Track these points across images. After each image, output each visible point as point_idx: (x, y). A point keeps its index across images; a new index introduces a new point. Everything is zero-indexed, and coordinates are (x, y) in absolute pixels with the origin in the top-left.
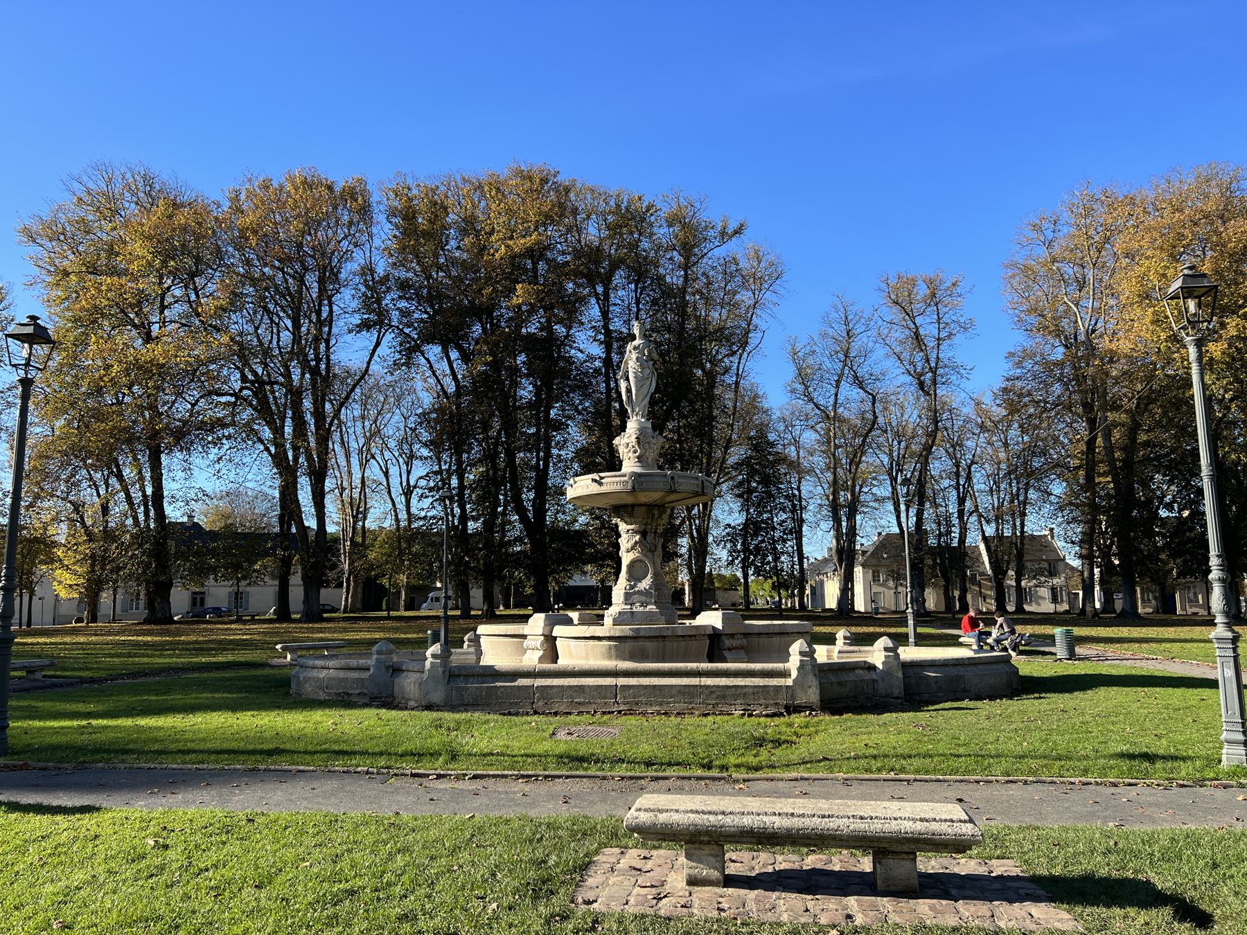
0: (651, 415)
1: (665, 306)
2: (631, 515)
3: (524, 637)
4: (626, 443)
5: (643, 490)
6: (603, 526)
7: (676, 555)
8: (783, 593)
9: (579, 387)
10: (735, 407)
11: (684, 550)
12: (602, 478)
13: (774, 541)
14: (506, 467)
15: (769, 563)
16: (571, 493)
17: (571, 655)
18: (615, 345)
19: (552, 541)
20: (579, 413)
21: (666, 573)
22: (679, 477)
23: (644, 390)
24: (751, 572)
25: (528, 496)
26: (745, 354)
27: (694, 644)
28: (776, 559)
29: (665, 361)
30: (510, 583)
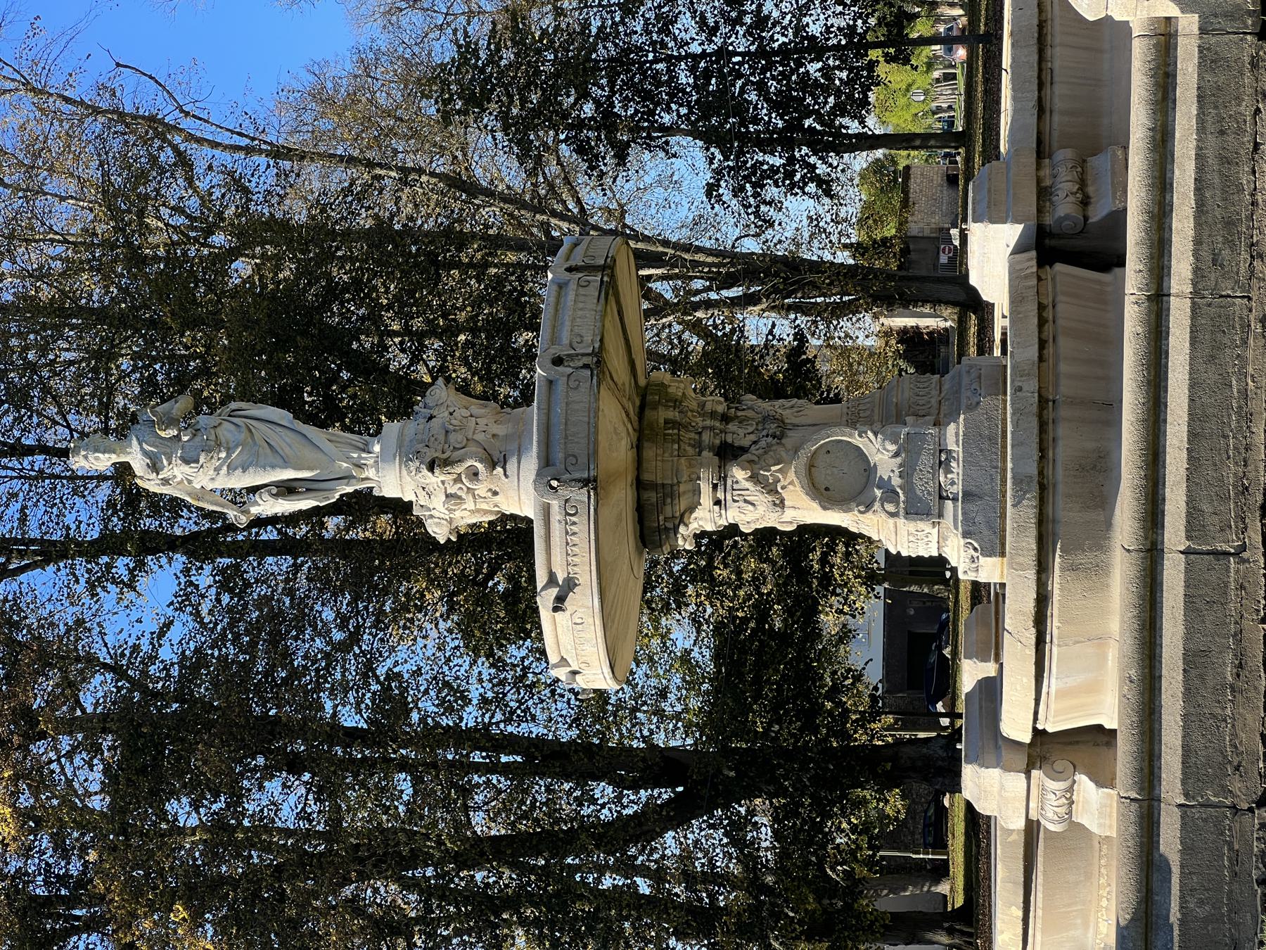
0: (363, 422)
1: (33, 367)
2: (668, 492)
3: (1032, 830)
4: (447, 505)
5: (593, 454)
6: (704, 575)
7: (797, 352)
8: (920, 29)
9: (276, 639)
10: (351, 161)
11: (785, 329)
12: (552, 580)
13: (762, 52)
14: (513, 866)
15: (827, 72)
16: (596, 676)
17: (1093, 688)
18: (148, 523)
19: (745, 731)
20: (355, 638)
21: (853, 384)
22: (554, 340)
23: (282, 440)
24: (854, 127)
25: (606, 801)
26: (186, 124)
27: (1066, 311)
28: (816, 48)
29: (204, 372)
30: (870, 863)
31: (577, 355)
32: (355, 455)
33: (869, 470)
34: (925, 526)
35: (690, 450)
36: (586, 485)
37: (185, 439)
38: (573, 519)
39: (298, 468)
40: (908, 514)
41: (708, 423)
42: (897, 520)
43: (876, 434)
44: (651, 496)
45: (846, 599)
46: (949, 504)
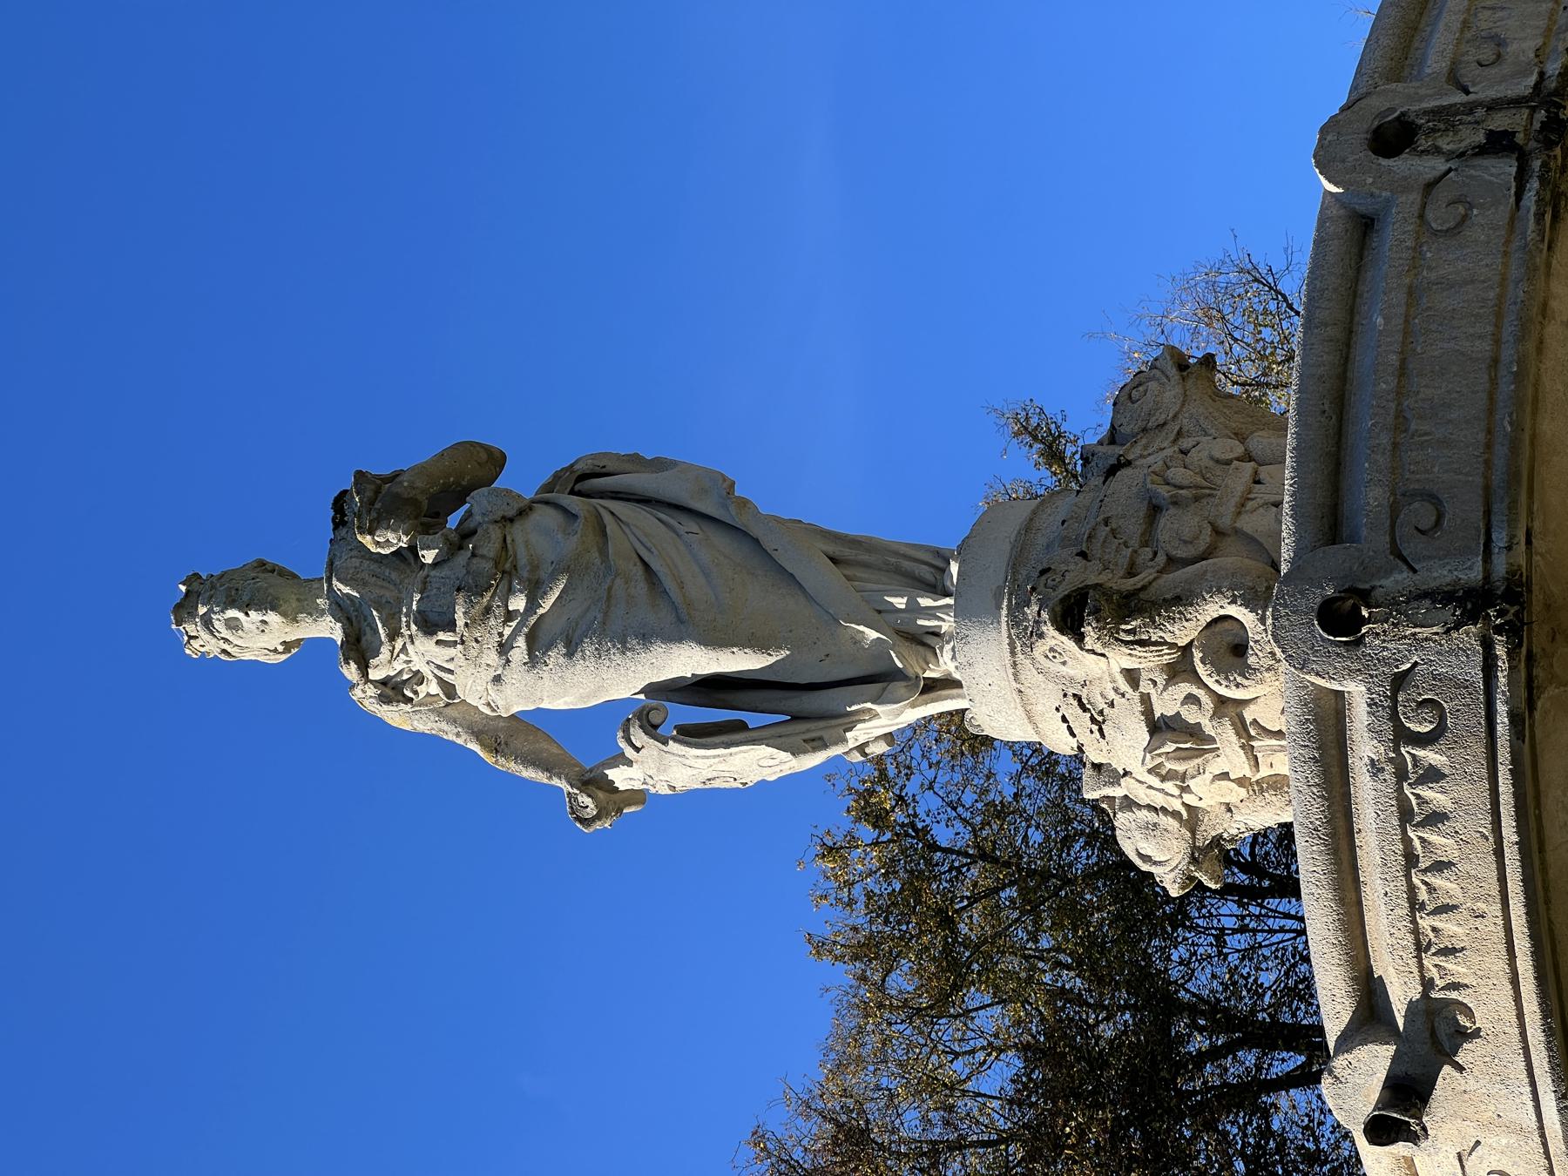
31: (1470, 108)
32: (900, 602)
36: (1471, 617)
37: (429, 556)
38: (1430, 756)
39: (714, 639)
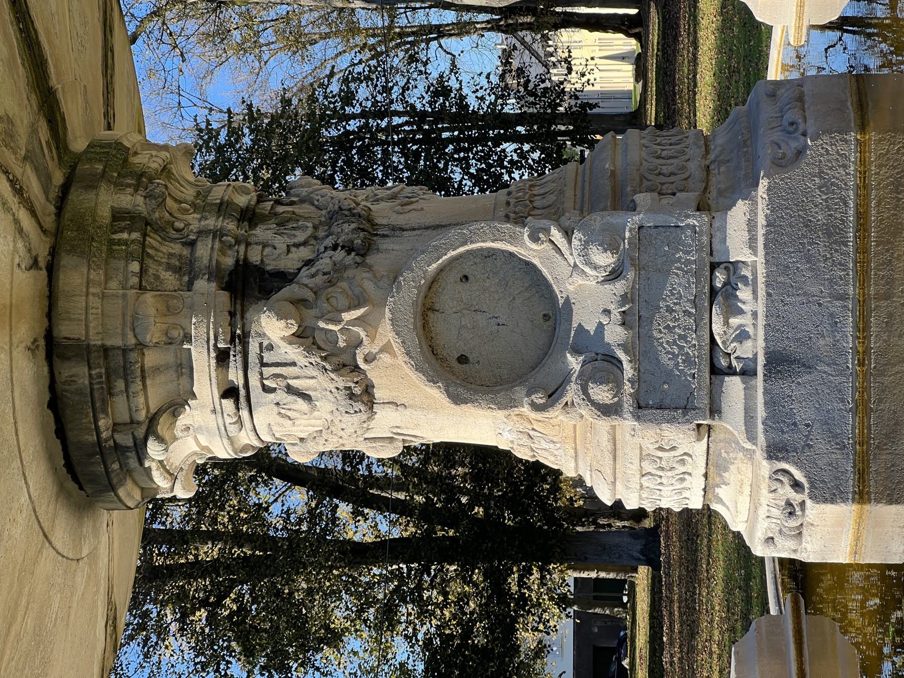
2: (117, 365)
33: (553, 313)
34: (680, 436)
35: (169, 279)
40: (641, 408)
41: (211, 222)
42: (616, 421)
43: (568, 234)
44: (78, 374)
45: (540, 618)
46: (734, 386)
